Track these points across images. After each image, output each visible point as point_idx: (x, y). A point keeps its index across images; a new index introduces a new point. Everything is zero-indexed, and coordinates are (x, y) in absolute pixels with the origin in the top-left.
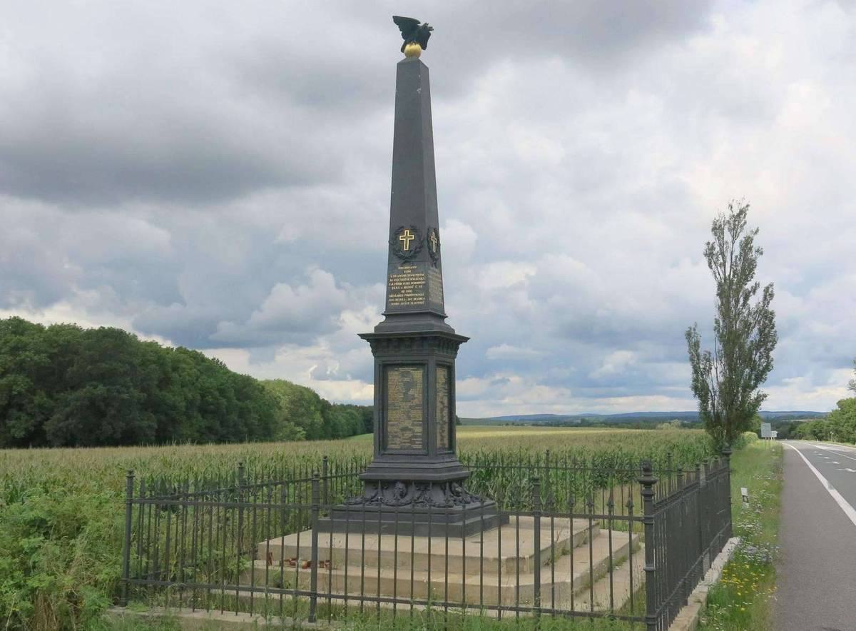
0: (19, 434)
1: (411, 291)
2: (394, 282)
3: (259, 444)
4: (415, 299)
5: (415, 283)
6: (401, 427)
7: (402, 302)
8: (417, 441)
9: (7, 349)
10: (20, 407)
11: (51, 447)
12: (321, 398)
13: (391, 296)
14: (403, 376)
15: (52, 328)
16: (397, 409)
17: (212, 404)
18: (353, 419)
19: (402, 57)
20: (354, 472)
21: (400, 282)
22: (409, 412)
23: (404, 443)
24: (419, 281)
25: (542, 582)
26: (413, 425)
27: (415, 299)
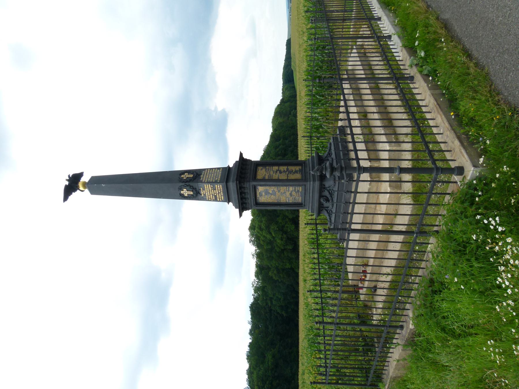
0: (293, 227)
1: (215, 191)
2: (211, 198)
3: (300, 248)
4: (219, 189)
5: (210, 189)
6: (289, 196)
7: (221, 195)
8: (297, 189)
9: (261, 232)
10: (283, 226)
11: (299, 216)
12: (279, 103)
13: (218, 200)
14: (262, 195)
15: (253, 215)
16: (280, 198)
17: (282, 152)
18: (288, 88)
19: (87, 191)
20: (316, 261)
21: (210, 195)
22: (282, 193)
23: (298, 195)
24: (209, 187)
25: (376, 112)
26: (289, 191)
27: (219, 189)
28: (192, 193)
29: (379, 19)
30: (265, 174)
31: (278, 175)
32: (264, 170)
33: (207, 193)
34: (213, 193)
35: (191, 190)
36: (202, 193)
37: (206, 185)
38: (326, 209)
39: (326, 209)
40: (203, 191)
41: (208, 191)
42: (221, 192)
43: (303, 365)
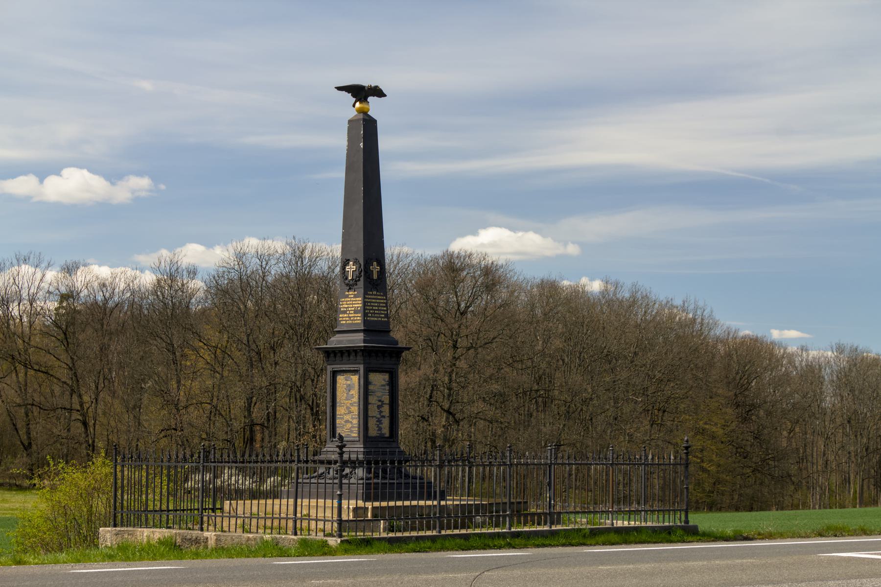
1: (353, 312)
5: (356, 305)
21: (347, 304)
31: (375, 404)
32: (383, 383)
35: (354, 278)
36: (350, 293)
40: (352, 294)
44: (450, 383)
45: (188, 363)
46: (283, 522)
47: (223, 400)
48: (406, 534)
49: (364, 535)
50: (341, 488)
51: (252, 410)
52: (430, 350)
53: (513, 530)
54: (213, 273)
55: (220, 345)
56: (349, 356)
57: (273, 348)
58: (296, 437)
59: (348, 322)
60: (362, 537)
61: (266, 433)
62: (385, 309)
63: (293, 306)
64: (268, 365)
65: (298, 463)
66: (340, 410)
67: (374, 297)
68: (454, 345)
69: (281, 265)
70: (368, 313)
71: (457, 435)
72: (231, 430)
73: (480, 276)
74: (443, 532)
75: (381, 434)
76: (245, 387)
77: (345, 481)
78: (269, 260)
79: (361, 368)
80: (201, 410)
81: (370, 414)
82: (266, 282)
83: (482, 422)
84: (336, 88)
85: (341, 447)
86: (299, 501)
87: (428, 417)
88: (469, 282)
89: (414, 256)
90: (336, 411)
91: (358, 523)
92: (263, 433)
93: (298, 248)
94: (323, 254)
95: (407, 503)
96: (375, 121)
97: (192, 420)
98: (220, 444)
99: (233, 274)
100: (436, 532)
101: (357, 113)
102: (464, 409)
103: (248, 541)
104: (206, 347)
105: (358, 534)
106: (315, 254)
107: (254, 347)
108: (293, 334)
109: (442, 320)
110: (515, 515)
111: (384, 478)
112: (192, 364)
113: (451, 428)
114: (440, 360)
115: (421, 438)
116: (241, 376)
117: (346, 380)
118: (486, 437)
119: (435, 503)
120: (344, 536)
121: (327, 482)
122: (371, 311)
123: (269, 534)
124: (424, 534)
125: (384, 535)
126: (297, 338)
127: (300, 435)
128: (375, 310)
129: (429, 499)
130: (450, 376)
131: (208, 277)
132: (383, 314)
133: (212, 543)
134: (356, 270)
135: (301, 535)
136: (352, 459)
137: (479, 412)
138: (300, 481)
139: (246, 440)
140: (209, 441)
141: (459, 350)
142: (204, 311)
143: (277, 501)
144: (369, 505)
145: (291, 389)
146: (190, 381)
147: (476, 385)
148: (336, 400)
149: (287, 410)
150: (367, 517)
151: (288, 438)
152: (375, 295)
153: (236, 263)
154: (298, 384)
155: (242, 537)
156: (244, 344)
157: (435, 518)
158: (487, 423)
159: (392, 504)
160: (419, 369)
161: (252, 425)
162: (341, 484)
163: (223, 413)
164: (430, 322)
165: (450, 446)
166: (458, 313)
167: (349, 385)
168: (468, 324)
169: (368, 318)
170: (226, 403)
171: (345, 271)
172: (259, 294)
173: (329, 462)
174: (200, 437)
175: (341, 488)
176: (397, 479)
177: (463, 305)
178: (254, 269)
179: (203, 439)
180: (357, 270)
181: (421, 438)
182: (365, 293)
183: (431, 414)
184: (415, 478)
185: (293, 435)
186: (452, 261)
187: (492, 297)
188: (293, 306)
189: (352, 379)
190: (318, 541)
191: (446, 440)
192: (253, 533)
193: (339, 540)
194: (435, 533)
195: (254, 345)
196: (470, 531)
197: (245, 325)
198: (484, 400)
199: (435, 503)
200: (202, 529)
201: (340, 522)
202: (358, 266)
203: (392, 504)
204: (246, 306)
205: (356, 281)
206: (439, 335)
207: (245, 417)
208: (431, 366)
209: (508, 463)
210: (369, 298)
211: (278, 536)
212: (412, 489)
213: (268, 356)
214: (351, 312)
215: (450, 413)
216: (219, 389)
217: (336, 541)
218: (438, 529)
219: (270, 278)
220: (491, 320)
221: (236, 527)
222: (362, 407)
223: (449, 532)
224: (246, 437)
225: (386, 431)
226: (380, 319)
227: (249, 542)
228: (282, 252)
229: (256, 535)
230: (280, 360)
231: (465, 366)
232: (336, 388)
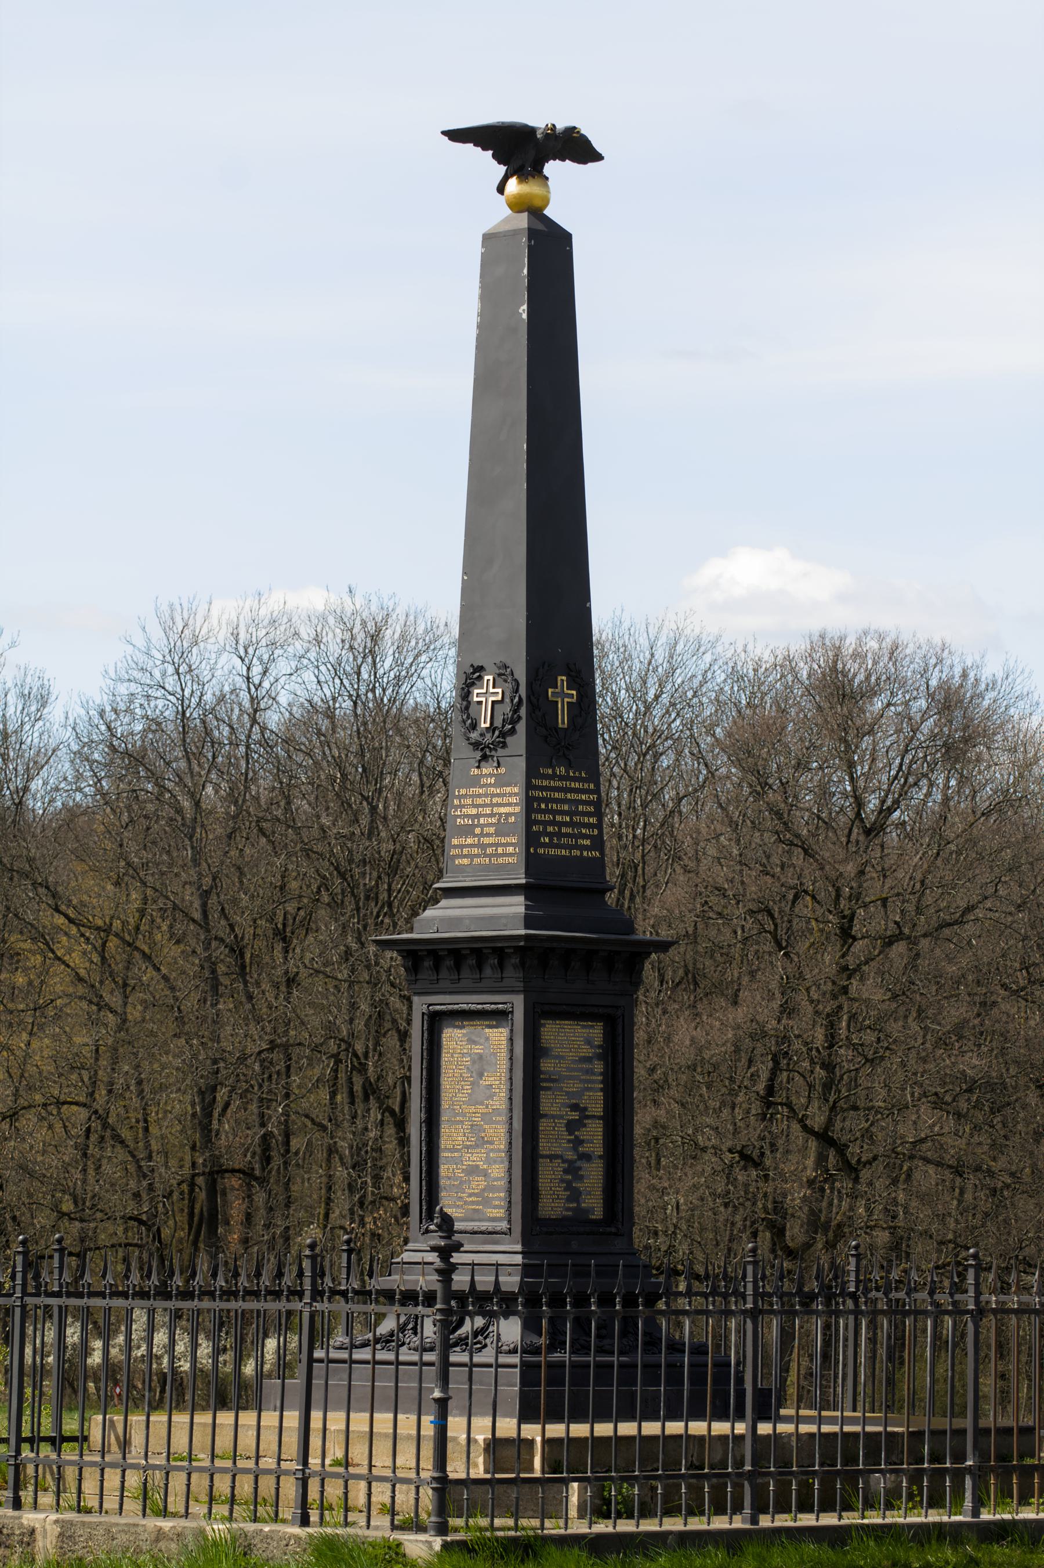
1: (492, 830)
4: (500, 850)
5: (503, 810)
24: (509, 805)
27: (500, 850)
28: (483, 725)
29: (840, 1518)
30: (562, 1057)
31: (561, 1117)
32: (587, 1051)
33: (486, 795)
34: (482, 821)
35: (498, 723)
36: (485, 771)
37: (516, 794)
38: (411, 1326)
39: (411, 1326)
40: (491, 775)
41: (495, 800)
42: (486, 855)
43: (362, 1454)
44: (831, 1046)
45: (20, 980)
46: (267, 1484)
47: (127, 1095)
48: (649, 1526)
49: (516, 1528)
50: (444, 1380)
51: (215, 1125)
52: (769, 946)
53: (986, 1516)
54: (98, 701)
55: (117, 924)
56: (480, 967)
57: (282, 936)
58: (352, 1212)
59: (476, 861)
60: (512, 1533)
61: (260, 1198)
62: (593, 820)
63: (346, 805)
64: (266, 986)
65: (313, 1299)
66: (450, 1136)
67: (559, 784)
68: (842, 928)
69: (309, 676)
70: (539, 834)
71: (851, 1209)
72: (151, 1188)
73: (925, 715)
74: (765, 1522)
75: (578, 1210)
76: (195, 1056)
77: (458, 1356)
78: (272, 659)
79: (518, 1003)
80: (58, 1127)
81: (545, 1146)
82: (263, 729)
83: (931, 1170)
84: (444, 133)
85: (445, 1252)
86: (316, 1416)
87: (762, 1154)
88: (887, 739)
89: (719, 649)
90: (439, 1137)
91: (500, 1489)
92: (249, 1196)
93: (364, 623)
94: (438, 644)
95: (651, 1428)
96: (566, 238)
97: (29, 1156)
98: (109, 1232)
99: (160, 703)
100: (743, 1521)
101: (508, 212)
102: (874, 1129)
103: (157, 1540)
104: (74, 930)
105: (497, 1522)
106: (413, 643)
107: (220, 928)
108: (343, 891)
109: (806, 851)
110: (992, 1469)
111: (580, 1347)
112: (30, 983)
113: (832, 1189)
114: (801, 976)
115: (738, 1218)
116: (180, 1020)
117: (471, 1041)
118: (942, 1218)
119: (741, 1428)
120: (456, 1530)
121: (401, 1358)
122: (550, 829)
123: (223, 1520)
124: (704, 1527)
125: (579, 1527)
126: (357, 903)
127: (361, 1204)
128: (561, 824)
129: (721, 1415)
130: (832, 1025)
131: (83, 712)
132: (585, 837)
133: (46, 1545)
134: (502, 701)
135: (322, 1521)
136: (479, 1288)
137: (922, 1141)
138: (319, 1354)
139: (196, 1219)
140: (82, 1220)
141: (859, 945)
142: (72, 815)
143: (248, 1418)
144: (532, 1431)
145: (338, 1062)
146: (25, 1036)
147: (913, 1054)
148: (439, 1105)
149: (324, 1128)
150: (531, 1469)
151: (327, 1216)
152: (561, 778)
153: (170, 669)
154: (359, 1048)
155: (140, 1529)
156: (194, 920)
157: (740, 1475)
158: (948, 1175)
159: (604, 1429)
160: (735, 1003)
161: (216, 1173)
162: (445, 1365)
163: (126, 1134)
164: (768, 857)
165: (830, 1246)
166: (855, 830)
167: (481, 1057)
168: (888, 862)
169: (541, 851)
170: (136, 1102)
171: (469, 703)
172: (237, 767)
173: (409, 1297)
174: (56, 1208)
175: (444, 1380)
176: (621, 1353)
177: (872, 803)
178: (227, 689)
179: (64, 1214)
180: (507, 700)
181: (738, 1218)
182: (532, 772)
183: (772, 1145)
184: (676, 1347)
185: (342, 1202)
186: (840, 666)
187: (963, 780)
188: (346, 805)
189: (487, 1039)
190: (373, 1545)
191: (815, 1223)
192: (174, 1515)
193: (437, 1543)
194: (738, 1523)
195: (223, 922)
196: (850, 1519)
197: (196, 862)
198: (938, 1103)
199: (741, 1428)
200: (17, 1504)
201: (443, 1485)
202: (509, 686)
203: (604, 1429)
204: (197, 804)
205: (503, 735)
206: (796, 897)
207: (193, 1148)
208: (772, 997)
209: (972, 1307)
210: (542, 788)
211: (250, 1527)
212: (668, 1383)
213: (267, 959)
214: (486, 830)
215: (831, 1142)
216: (115, 1061)
217: (429, 1544)
218: (747, 1511)
219: (276, 717)
220: (959, 853)
221: (122, 1497)
222: (518, 1125)
223: (783, 1521)
224: (197, 1211)
225: (594, 1203)
226: (576, 853)
227: (162, 1545)
228: (313, 634)
229: (183, 1523)
230: (302, 970)
231: (878, 996)
232: (439, 1067)
